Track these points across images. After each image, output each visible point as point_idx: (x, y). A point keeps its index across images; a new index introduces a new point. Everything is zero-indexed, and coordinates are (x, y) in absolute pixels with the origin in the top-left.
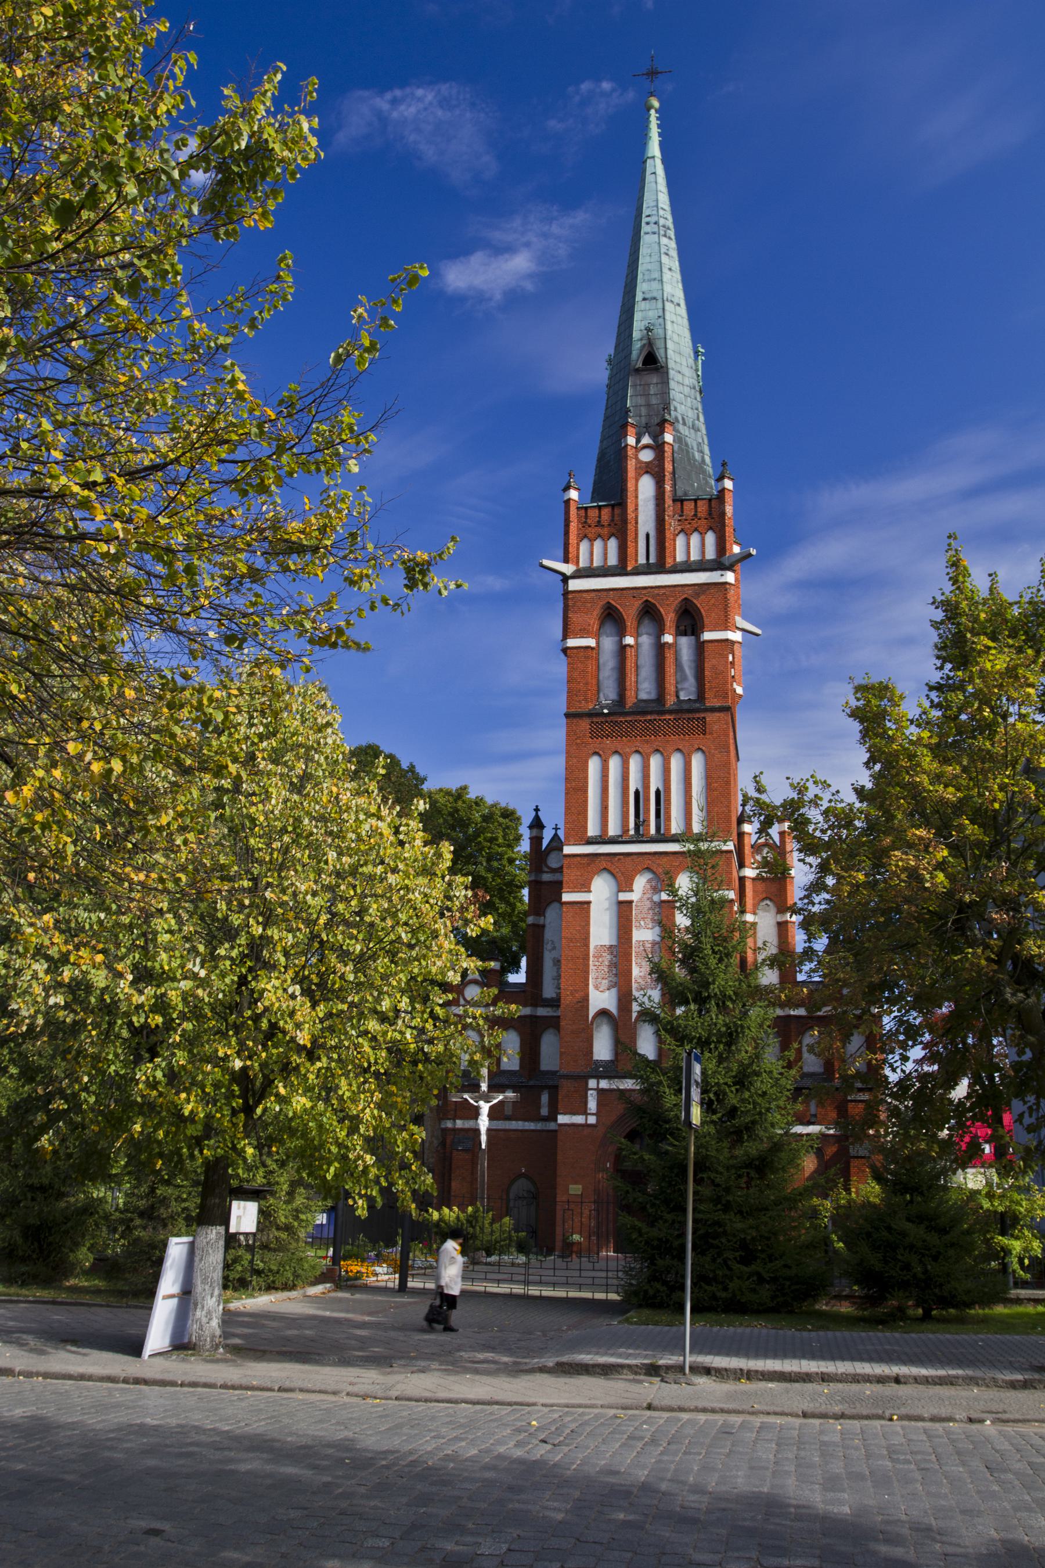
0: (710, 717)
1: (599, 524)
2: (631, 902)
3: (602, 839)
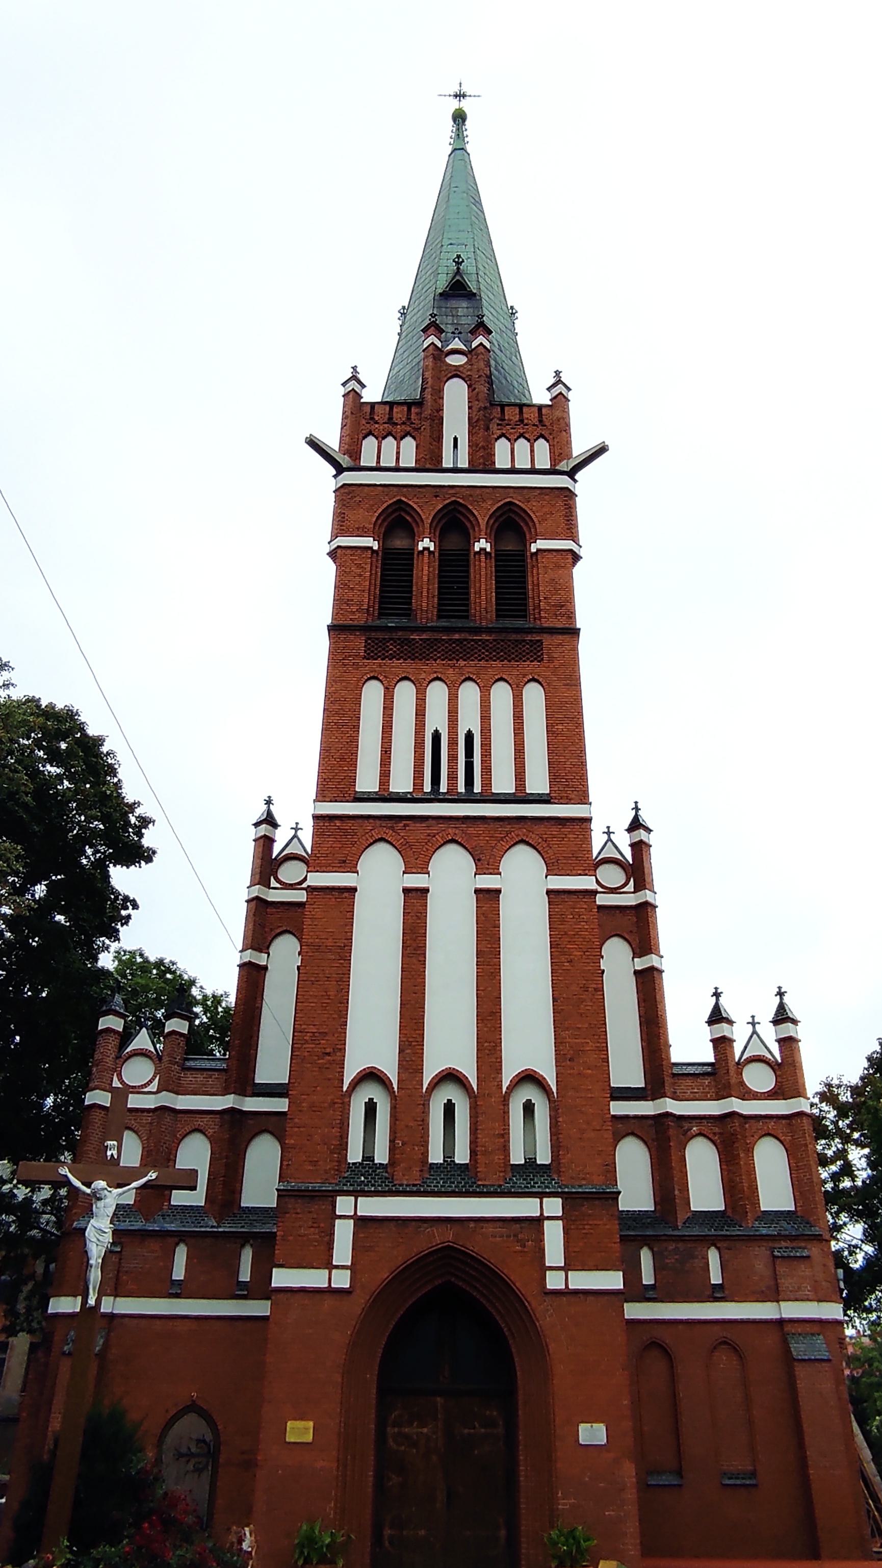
0: (547, 640)
1: (390, 420)
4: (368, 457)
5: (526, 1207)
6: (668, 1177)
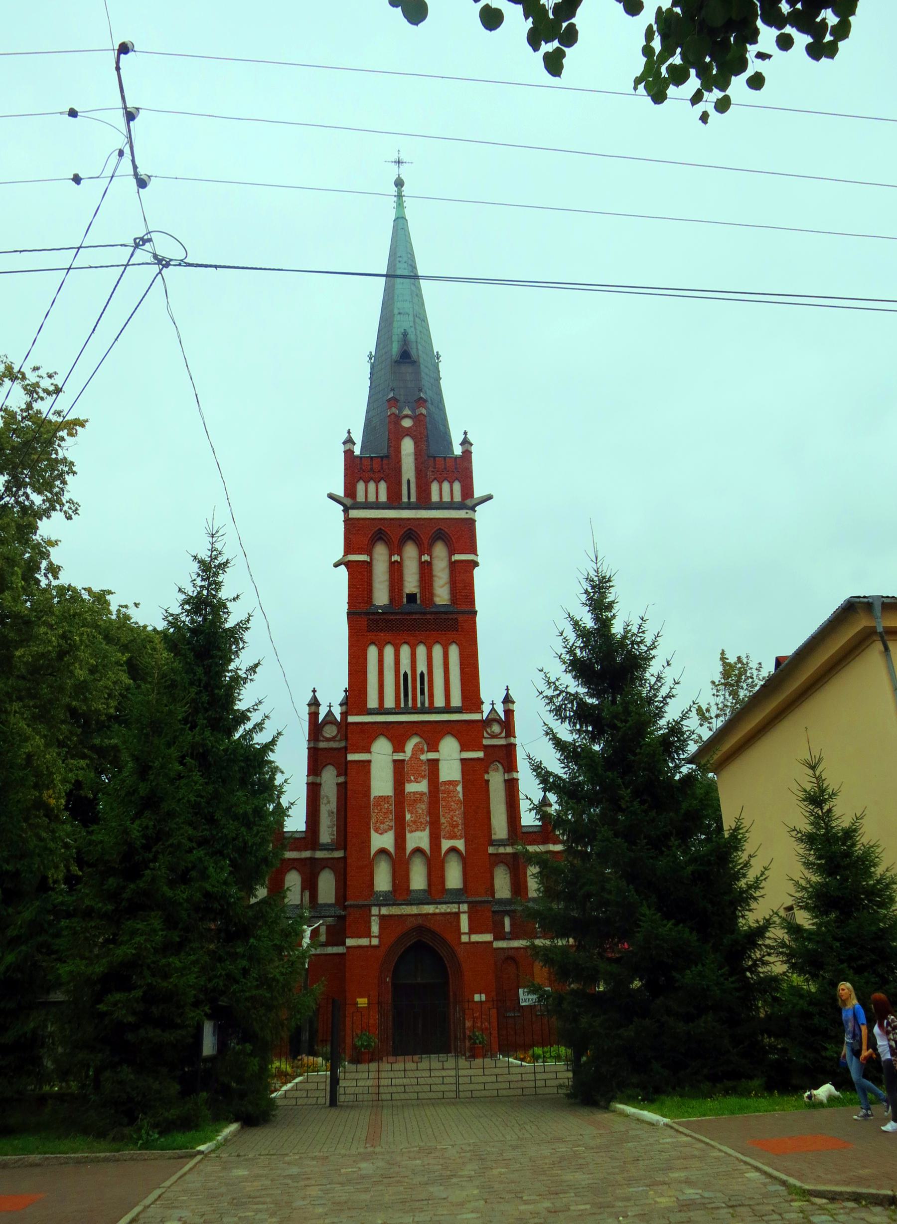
2: (403, 761)
3: (448, 709)
4: (361, 497)
5: (453, 908)
6: (518, 886)
